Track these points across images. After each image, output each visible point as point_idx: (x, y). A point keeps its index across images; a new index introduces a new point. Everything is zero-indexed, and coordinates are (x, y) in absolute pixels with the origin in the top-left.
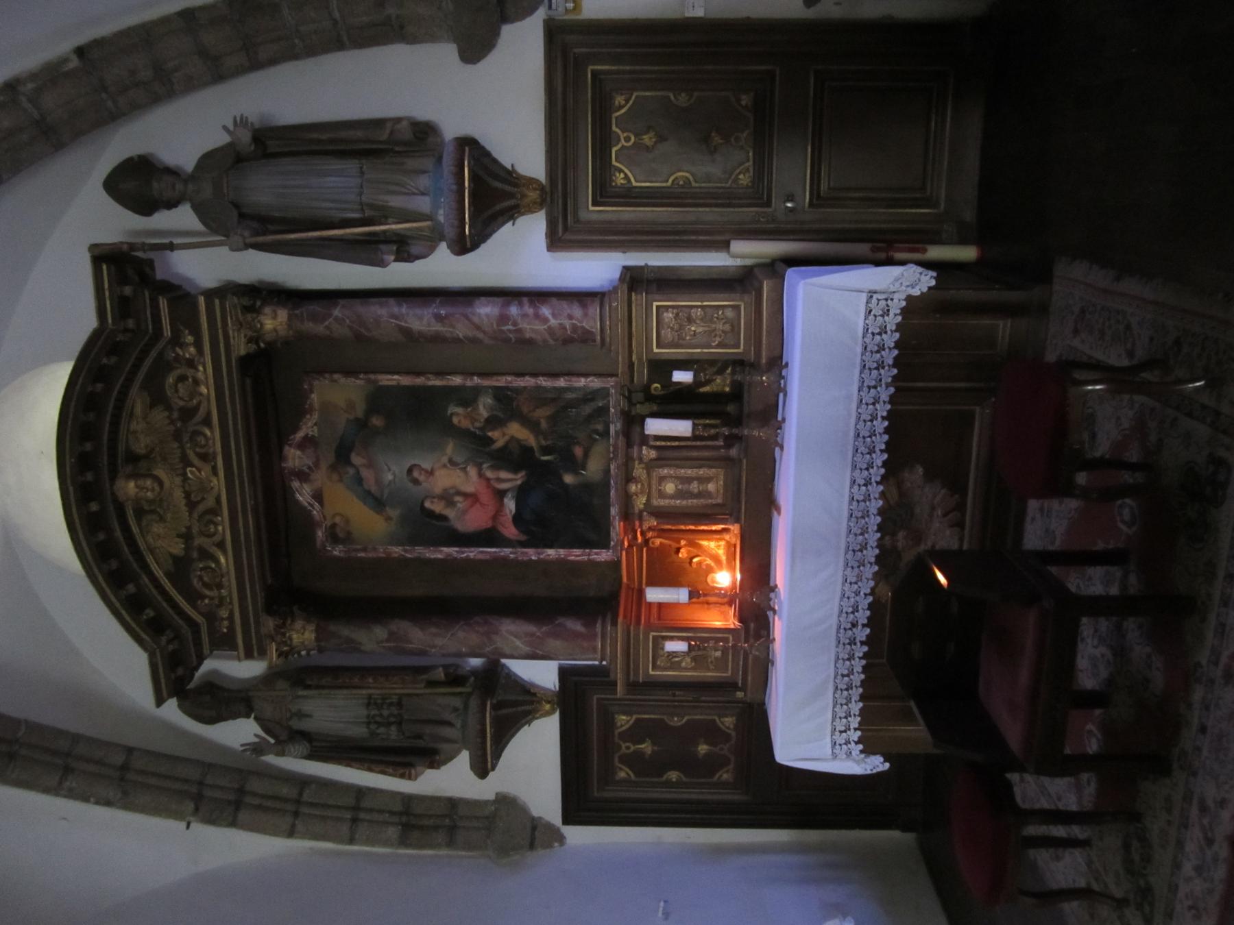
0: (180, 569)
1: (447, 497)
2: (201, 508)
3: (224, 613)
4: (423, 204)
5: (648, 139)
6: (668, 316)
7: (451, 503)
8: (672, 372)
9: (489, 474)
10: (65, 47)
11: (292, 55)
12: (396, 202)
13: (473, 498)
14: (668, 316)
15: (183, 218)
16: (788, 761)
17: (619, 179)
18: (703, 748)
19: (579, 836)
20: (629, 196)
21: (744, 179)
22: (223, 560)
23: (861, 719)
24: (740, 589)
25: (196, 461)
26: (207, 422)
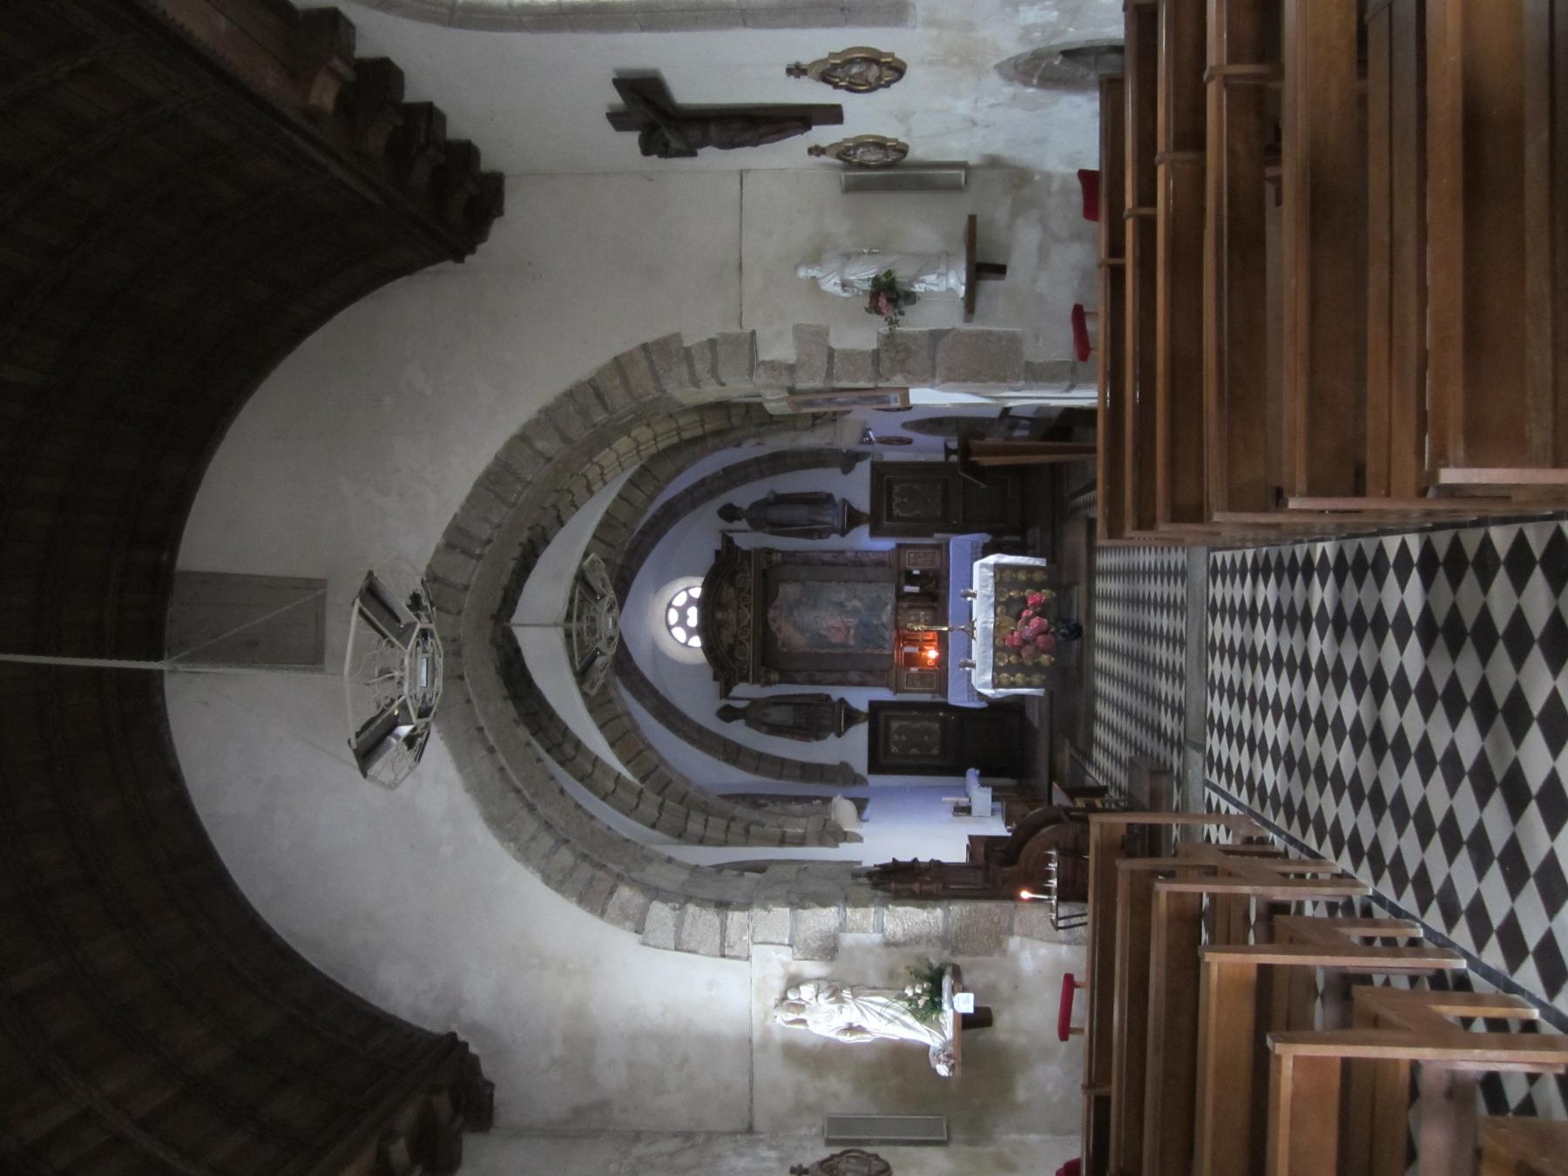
0: (732, 648)
1: (829, 629)
2: (741, 626)
3: (745, 667)
4: (828, 519)
5: (905, 500)
6: (912, 555)
7: (829, 631)
8: (831, 732)
9: (846, 620)
10: (719, 468)
11: (786, 471)
12: (819, 519)
13: (838, 629)
14: (912, 555)
15: (742, 524)
16: (961, 702)
17: (895, 513)
18: (926, 738)
19: (876, 780)
20: (899, 519)
21: (939, 513)
22: (748, 646)
23: (987, 773)
24: (975, 463)
25: (743, 607)
26: (749, 592)
